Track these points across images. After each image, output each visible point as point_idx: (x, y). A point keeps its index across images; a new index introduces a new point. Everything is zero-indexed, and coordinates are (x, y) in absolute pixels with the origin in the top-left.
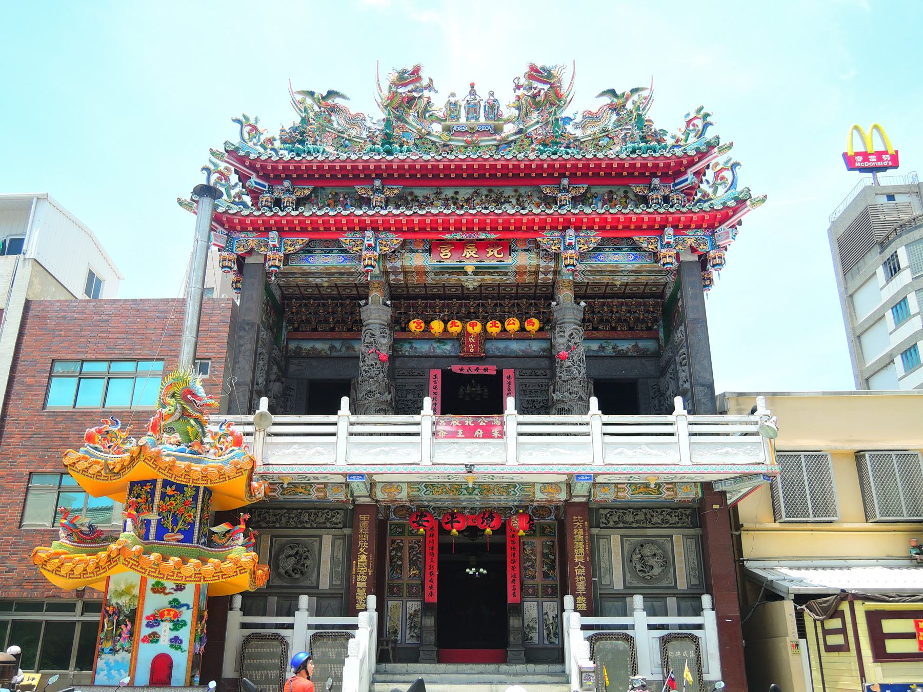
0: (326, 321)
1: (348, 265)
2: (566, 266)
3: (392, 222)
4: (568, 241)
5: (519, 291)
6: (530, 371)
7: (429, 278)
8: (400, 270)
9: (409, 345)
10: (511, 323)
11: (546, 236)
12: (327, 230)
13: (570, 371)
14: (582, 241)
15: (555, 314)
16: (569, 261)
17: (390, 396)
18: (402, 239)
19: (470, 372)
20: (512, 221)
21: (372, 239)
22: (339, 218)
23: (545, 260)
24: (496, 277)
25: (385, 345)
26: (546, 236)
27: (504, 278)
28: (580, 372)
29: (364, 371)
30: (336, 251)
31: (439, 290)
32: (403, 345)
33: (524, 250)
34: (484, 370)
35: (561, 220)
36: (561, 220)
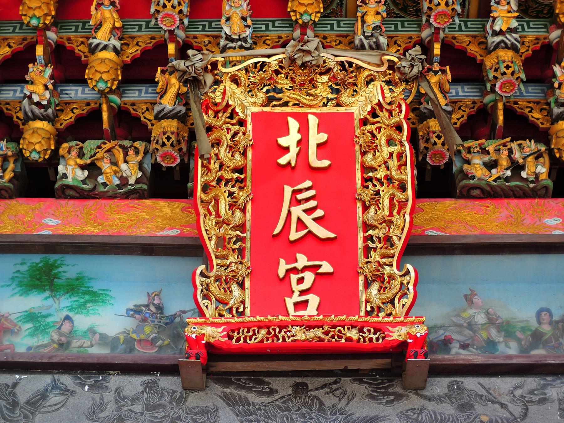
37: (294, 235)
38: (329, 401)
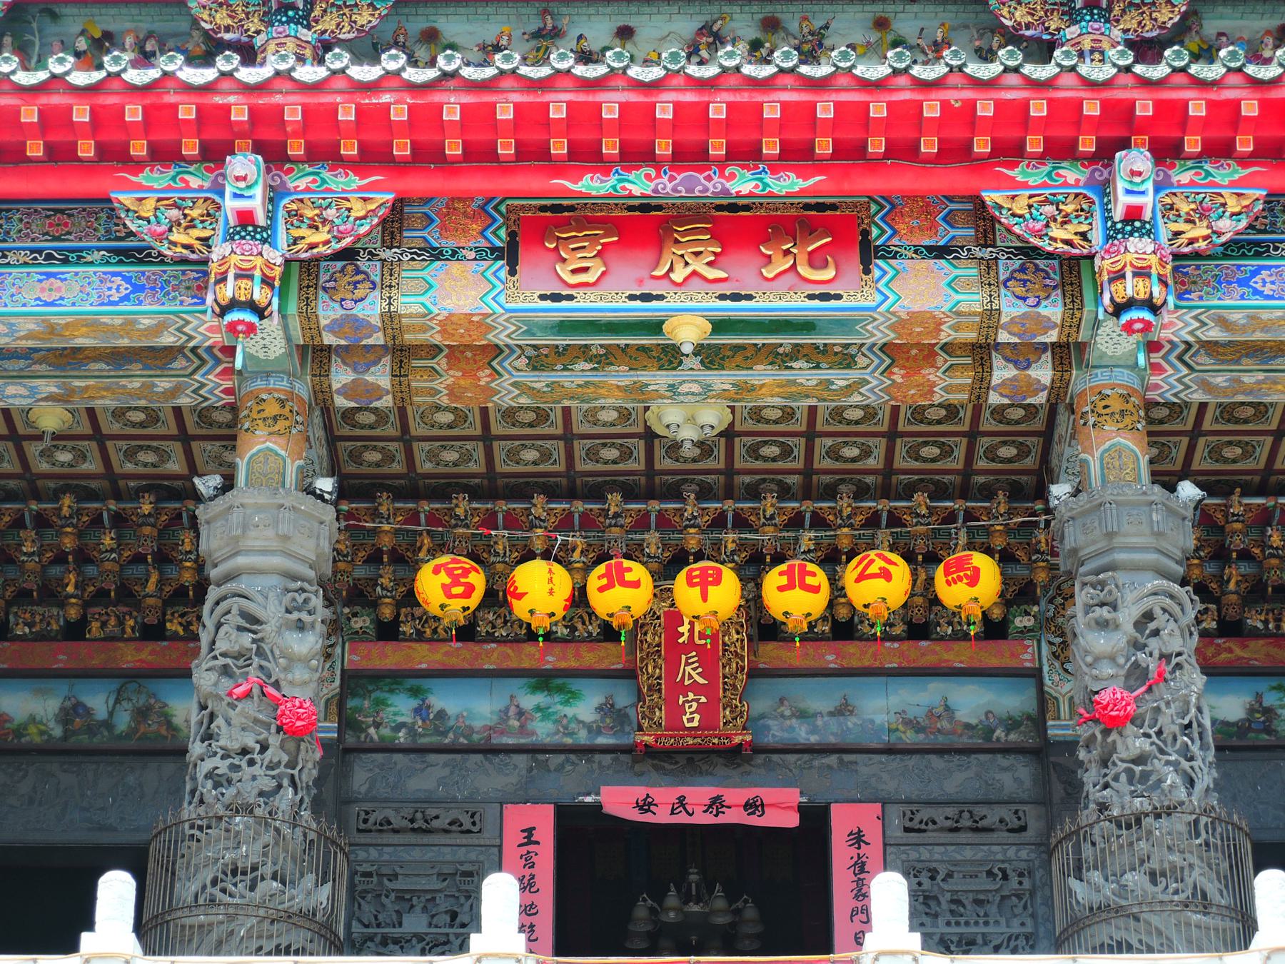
0: (51, 594)
1: (147, 311)
2: (1118, 309)
3: (347, 114)
4: (1123, 200)
5: (899, 463)
6: (951, 811)
7: (506, 382)
8: (378, 339)
9: (414, 703)
10: (874, 569)
11: (1025, 186)
12: (61, 154)
13: (1145, 776)
14: (1185, 208)
15: (1069, 530)
16: (1131, 287)
17: (327, 890)
18: (390, 196)
19: (682, 818)
20: (878, 110)
21: (258, 191)
22: (111, 100)
23: (1020, 291)
24: (804, 375)
25: (305, 661)
26: (1025, 186)
27: (840, 378)
28: (1191, 783)
29: (209, 775)
30: (97, 256)
31: (546, 456)
32: (381, 703)
33: (930, 249)
34: (747, 806)
35: (1092, 109)
36: (1092, 109)
37: (687, 683)
38: (705, 767)
